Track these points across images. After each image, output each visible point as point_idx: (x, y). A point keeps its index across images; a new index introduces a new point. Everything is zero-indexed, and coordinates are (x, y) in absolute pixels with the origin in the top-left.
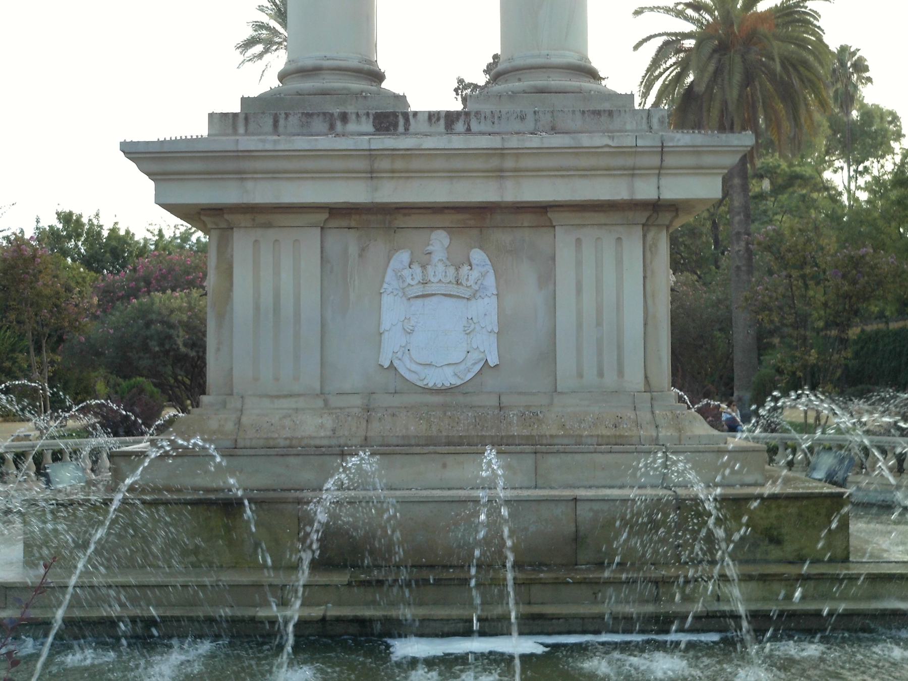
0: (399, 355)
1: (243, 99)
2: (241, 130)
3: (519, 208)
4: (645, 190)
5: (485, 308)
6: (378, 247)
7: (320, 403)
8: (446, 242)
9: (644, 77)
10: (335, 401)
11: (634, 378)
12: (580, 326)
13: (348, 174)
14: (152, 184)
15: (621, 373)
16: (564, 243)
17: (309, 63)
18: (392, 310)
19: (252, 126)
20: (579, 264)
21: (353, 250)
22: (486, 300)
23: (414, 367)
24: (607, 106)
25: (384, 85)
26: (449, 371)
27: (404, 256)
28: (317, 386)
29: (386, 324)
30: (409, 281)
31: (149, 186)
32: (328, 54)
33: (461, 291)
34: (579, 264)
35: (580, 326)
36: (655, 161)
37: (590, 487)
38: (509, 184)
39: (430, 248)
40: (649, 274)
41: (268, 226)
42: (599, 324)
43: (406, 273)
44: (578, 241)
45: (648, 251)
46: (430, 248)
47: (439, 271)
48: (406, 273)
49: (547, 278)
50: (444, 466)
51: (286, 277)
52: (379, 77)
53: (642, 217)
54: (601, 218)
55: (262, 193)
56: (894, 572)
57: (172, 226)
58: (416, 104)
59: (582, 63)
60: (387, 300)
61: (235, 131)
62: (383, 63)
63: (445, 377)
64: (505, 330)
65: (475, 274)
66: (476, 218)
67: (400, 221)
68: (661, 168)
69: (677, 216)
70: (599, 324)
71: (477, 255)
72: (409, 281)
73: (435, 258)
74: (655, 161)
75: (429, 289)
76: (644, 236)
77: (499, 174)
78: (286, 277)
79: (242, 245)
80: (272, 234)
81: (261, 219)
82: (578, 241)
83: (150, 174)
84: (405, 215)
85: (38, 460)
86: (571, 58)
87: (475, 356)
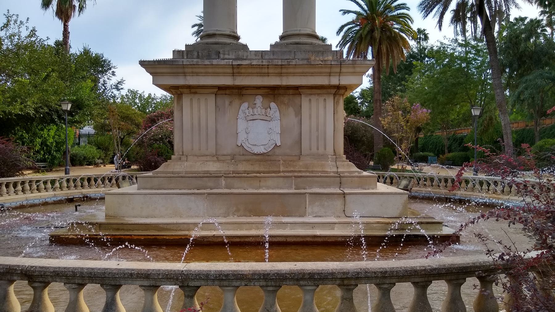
0: (244, 141)
1: (186, 45)
2: (185, 57)
3: (288, 88)
4: (334, 81)
5: (276, 125)
6: (236, 102)
7: (215, 158)
8: (261, 100)
9: (340, 42)
10: (221, 158)
11: (330, 150)
12: (310, 131)
13: (224, 74)
14: (151, 77)
15: (325, 149)
16: (305, 101)
17: (211, 32)
18: (242, 125)
19: (189, 56)
20: (310, 109)
21: (227, 102)
22: (276, 121)
23: (250, 146)
24: (321, 49)
25: (240, 41)
26: (262, 147)
27: (245, 105)
28: (214, 152)
29: (239, 130)
30: (248, 114)
31: (150, 77)
32: (219, 29)
33: (268, 119)
34: (310, 109)
35: (310, 131)
36: (338, 70)
37: (22, 207)
38: (284, 78)
39: (255, 102)
40: (336, 112)
41: (195, 93)
42: (317, 130)
43: (247, 111)
44: (310, 100)
45: (336, 104)
46: (255, 102)
47: (259, 111)
48: (247, 111)
49: (299, 113)
50: (260, 181)
51: (203, 112)
52: (238, 38)
53: (333, 91)
54: (318, 91)
55: (192, 81)
56: (255, 263)
57: (159, 93)
58: (251, 48)
59: (313, 33)
60: (239, 121)
61: (183, 58)
62: (239, 33)
63: (261, 150)
64: (282, 133)
65: (272, 112)
66: (273, 93)
67: (244, 92)
68: (340, 73)
69: (346, 91)
70: (317, 130)
71: (273, 105)
72: (248, 114)
73: (257, 106)
74: (338, 70)
75: (255, 117)
76: (334, 98)
77: (280, 74)
78: (203, 112)
79: (186, 101)
80: (197, 96)
81: (193, 90)
82: (310, 100)
83: (151, 74)
84: (246, 89)
85: (117, 180)
86: (309, 31)
87: (273, 142)
